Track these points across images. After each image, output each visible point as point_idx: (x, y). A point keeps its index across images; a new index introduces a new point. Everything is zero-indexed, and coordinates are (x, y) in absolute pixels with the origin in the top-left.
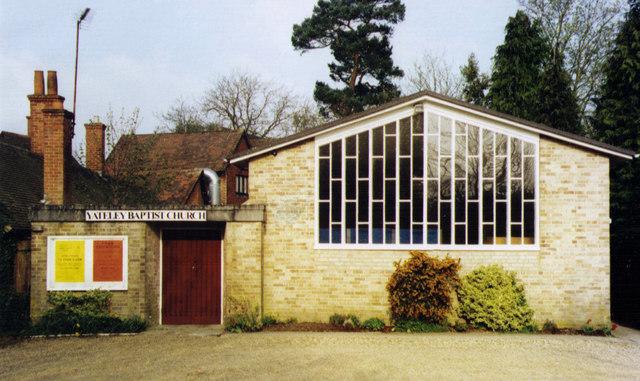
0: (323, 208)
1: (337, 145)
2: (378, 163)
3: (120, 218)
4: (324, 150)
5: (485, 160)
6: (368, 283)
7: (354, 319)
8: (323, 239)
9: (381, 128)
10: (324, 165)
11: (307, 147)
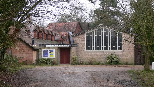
0: (87, 44)
1: (89, 33)
2: (96, 36)
3: (50, 46)
4: (87, 34)
5: (111, 32)
6: (94, 57)
7: (99, 62)
8: (87, 49)
9: (96, 30)
10: (87, 37)
11: (84, 35)
